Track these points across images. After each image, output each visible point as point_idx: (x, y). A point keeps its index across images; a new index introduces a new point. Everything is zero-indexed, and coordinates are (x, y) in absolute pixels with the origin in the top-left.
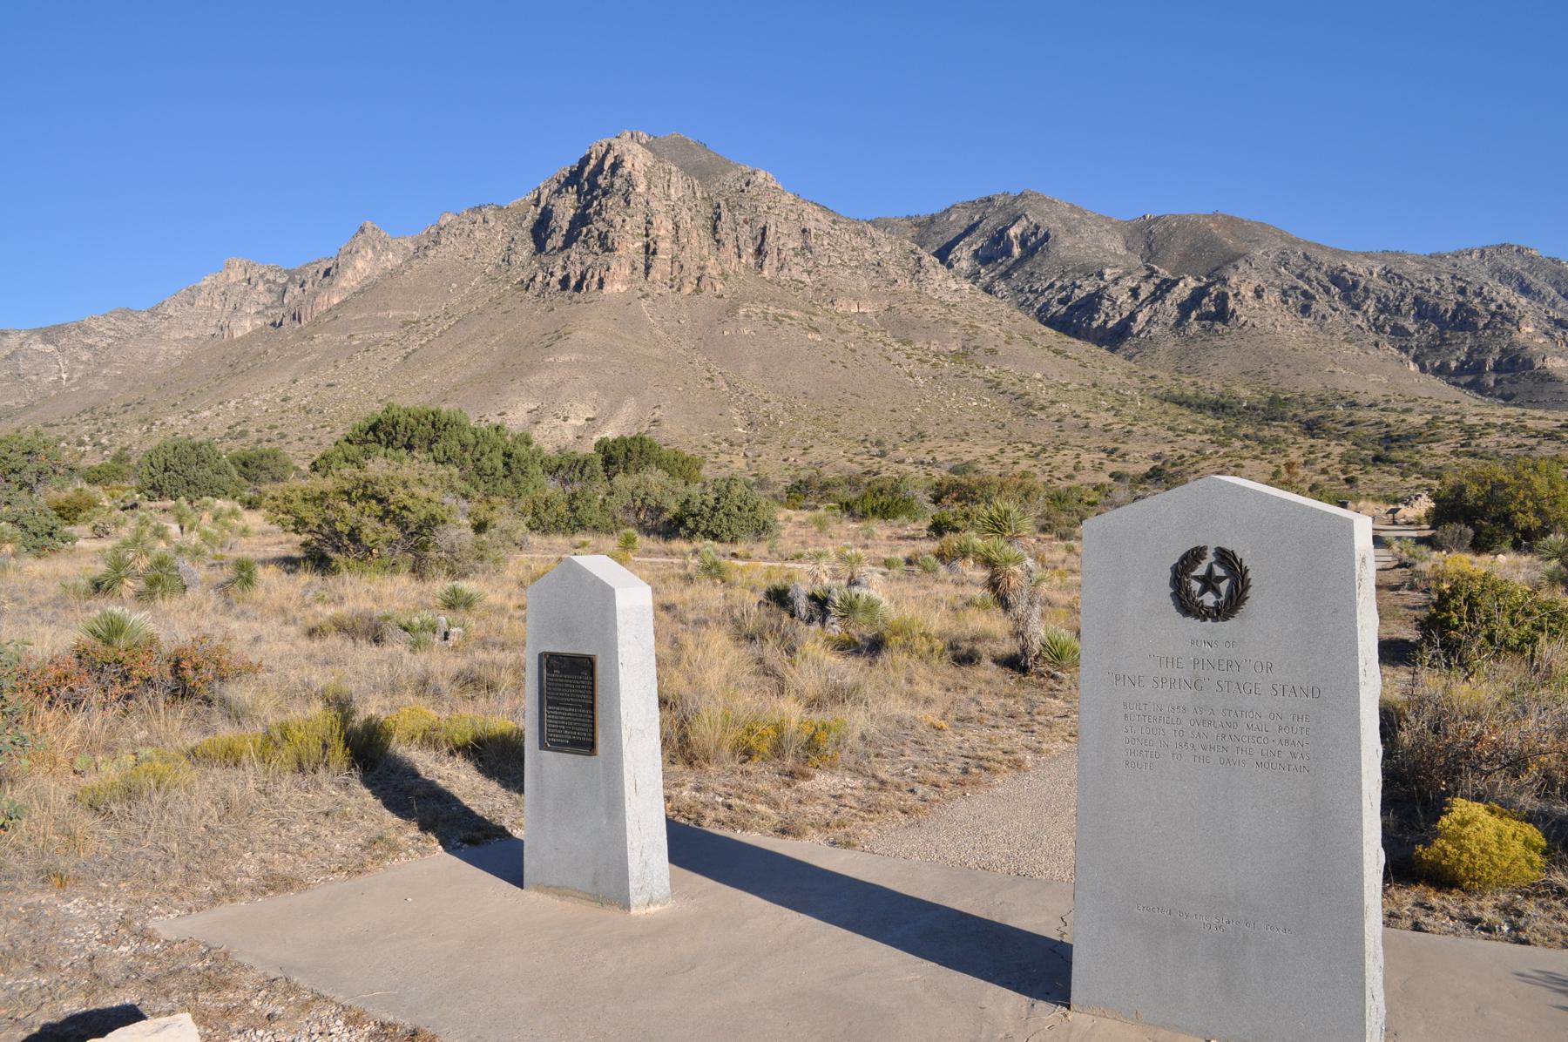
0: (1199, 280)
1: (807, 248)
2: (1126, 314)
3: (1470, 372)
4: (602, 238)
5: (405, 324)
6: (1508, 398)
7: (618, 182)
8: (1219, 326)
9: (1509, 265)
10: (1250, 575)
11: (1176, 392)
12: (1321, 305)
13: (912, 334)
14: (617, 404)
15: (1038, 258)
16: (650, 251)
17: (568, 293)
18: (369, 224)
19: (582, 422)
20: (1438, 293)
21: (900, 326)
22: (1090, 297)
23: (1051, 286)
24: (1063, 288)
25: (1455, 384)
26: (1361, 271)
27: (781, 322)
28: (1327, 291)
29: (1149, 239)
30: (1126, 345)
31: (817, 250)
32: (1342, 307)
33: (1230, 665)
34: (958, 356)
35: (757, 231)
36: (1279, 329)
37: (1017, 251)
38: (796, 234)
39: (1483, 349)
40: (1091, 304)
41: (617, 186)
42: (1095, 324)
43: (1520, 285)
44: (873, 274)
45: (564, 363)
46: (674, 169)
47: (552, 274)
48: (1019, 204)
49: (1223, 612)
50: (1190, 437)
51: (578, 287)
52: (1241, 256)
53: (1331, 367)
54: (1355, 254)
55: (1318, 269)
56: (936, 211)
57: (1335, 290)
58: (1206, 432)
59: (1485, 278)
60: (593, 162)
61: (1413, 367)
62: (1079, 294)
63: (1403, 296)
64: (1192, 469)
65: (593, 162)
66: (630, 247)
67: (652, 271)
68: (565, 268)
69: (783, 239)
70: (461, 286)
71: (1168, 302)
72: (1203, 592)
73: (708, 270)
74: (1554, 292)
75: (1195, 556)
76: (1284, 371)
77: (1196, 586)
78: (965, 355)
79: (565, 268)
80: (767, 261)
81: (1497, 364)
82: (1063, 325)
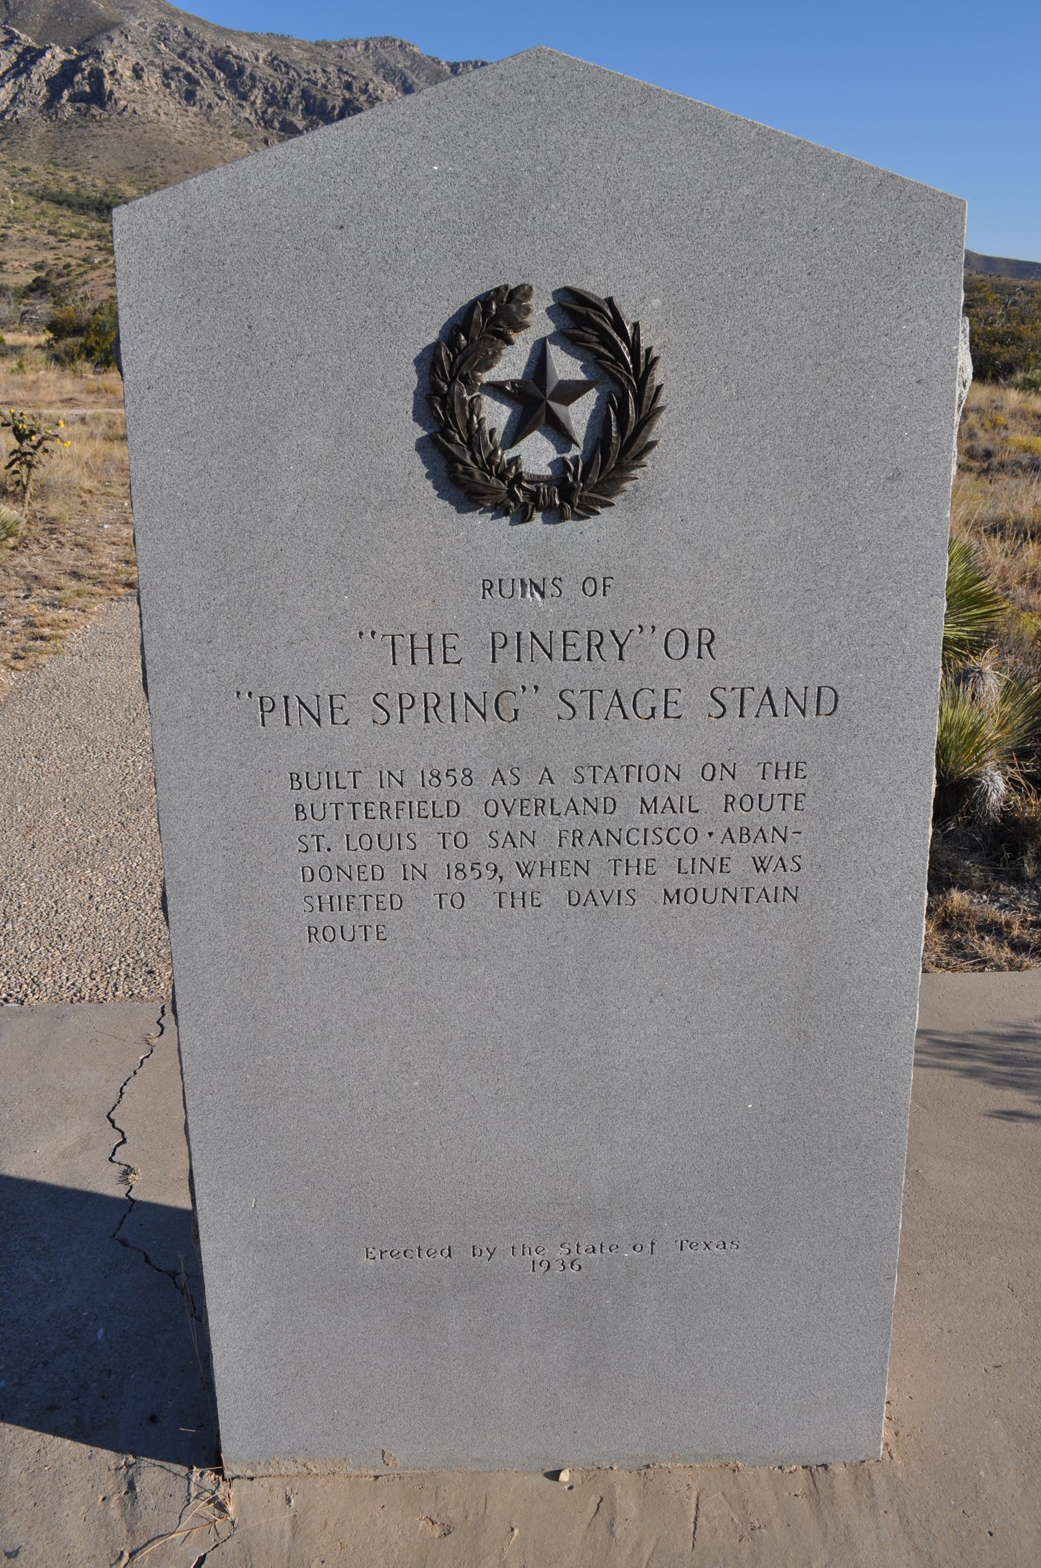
0: (68, 51)
8: (95, 110)
9: (392, 61)
10: (658, 377)
11: (54, 188)
12: (205, 91)
20: (325, 87)
26: (246, 55)
28: (212, 76)
32: (228, 95)
33: (594, 644)
36: (163, 118)
43: (404, 82)
49: (580, 490)
50: (75, 242)
52: (115, 25)
54: (240, 34)
55: (201, 49)
57: (220, 75)
58: (92, 237)
59: (370, 73)
63: (290, 87)
64: (81, 281)
71: (35, 77)
72: (517, 432)
75: (490, 318)
77: (496, 415)
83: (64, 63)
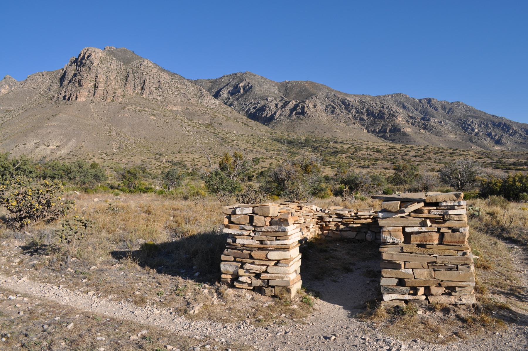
0: (297, 101)
1: (160, 87)
2: (273, 112)
3: (382, 132)
4: (79, 81)
5: (7, 111)
6: (393, 141)
7: (88, 62)
8: (302, 117)
9: (400, 100)
12: (337, 111)
13: (193, 117)
14: (69, 140)
15: (248, 93)
16: (96, 87)
17: (65, 101)
18: (8, 76)
19: (54, 147)
21: (190, 115)
22: (263, 106)
23: (251, 103)
24: (255, 104)
25: (378, 136)
27: (141, 112)
28: (341, 106)
29: (286, 88)
30: (272, 123)
31: (163, 88)
32: (345, 111)
34: (208, 125)
35: (142, 81)
36: (321, 118)
37: (242, 91)
38: (156, 82)
39: (386, 125)
40: (262, 109)
41: (87, 63)
42: (263, 116)
44: (183, 97)
45: (52, 126)
46: (114, 58)
47: (60, 94)
48: (244, 76)
51: (69, 99)
52: (314, 94)
53: (335, 130)
54: (351, 95)
55: (338, 99)
56: (218, 78)
60: (82, 55)
61: (365, 131)
62: (259, 106)
63: (363, 108)
65: (82, 55)
66: (88, 84)
67: (96, 94)
68: (65, 92)
69: (151, 84)
70: (30, 98)
71: (286, 109)
73: (117, 94)
74: (413, 108)
76: (320, 131)
78: (211, 125)
79: (65, 92)
80: (145, 92)
81: (390, 130)
82: (253, 116)
83: (295, 104)
